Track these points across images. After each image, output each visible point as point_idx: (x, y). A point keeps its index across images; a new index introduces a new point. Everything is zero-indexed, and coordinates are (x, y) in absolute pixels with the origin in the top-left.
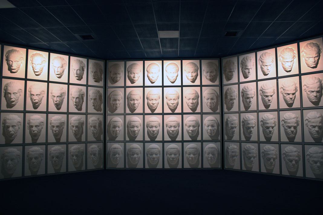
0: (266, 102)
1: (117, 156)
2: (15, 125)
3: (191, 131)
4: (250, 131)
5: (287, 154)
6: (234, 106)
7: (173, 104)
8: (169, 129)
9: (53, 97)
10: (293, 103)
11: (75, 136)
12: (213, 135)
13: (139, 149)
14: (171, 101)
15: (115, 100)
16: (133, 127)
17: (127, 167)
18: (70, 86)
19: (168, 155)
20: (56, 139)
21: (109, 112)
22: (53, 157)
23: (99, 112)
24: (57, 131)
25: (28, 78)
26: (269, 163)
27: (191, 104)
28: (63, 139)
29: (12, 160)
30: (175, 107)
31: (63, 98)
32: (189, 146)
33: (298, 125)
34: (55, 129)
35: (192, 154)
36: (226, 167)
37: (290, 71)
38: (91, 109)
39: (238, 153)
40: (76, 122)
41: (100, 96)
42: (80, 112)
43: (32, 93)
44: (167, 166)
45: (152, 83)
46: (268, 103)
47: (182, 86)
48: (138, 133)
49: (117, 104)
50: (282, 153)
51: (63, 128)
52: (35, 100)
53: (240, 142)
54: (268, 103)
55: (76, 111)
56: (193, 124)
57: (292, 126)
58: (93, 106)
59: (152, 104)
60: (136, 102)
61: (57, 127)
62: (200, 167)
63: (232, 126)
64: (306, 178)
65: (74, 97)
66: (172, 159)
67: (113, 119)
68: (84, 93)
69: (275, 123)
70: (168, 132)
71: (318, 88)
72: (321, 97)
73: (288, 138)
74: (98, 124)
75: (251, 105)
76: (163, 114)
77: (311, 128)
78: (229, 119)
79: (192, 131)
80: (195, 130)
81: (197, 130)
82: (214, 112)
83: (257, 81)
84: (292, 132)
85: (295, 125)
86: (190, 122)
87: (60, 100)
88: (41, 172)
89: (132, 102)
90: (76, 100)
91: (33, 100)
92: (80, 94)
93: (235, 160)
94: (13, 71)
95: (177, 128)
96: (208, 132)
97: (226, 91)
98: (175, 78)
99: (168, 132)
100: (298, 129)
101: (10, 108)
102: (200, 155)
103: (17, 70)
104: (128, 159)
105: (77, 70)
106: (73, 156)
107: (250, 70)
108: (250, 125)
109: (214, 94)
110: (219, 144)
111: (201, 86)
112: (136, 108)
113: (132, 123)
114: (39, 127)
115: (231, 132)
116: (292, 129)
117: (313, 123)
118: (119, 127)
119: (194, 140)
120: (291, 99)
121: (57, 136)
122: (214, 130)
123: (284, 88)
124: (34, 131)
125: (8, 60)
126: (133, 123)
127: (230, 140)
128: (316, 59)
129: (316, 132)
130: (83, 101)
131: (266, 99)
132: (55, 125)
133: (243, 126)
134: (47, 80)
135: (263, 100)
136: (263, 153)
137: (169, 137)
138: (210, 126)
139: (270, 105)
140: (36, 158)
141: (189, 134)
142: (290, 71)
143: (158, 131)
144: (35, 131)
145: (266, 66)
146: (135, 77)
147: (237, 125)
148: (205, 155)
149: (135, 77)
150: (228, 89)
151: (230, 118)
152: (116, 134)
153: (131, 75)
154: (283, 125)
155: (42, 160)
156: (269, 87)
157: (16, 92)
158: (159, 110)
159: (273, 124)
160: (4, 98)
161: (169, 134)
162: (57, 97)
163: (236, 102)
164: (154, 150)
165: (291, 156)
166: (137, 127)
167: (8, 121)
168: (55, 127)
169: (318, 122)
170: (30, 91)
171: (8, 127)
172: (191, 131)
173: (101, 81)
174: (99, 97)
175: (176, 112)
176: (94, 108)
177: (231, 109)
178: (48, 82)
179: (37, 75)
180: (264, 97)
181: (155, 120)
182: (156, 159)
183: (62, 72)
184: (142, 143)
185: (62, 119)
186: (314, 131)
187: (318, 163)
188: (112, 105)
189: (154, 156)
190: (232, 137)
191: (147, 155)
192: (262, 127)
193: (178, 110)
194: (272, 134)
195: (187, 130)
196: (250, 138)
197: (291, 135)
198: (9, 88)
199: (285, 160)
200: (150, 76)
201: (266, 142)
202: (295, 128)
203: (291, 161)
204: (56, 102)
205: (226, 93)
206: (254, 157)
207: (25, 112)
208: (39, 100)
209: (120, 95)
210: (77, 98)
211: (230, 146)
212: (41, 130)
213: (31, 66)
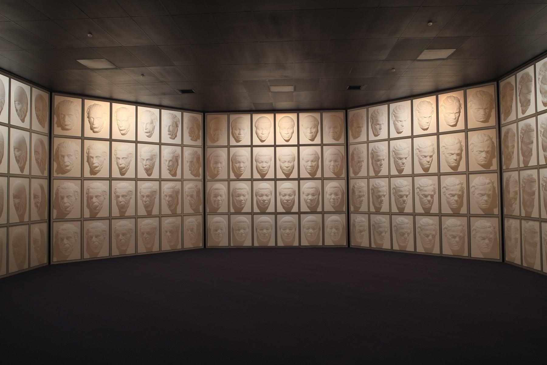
0: (399, 166)
1: (219, 231)
2: (100, 195)
3: (309, 201)
4: (380, 200)
5: (423, 227)
6: (362, 170)
7: (287, 167)
8: (283, 198)
10: (430, 167)
11: (169, 208)
12: (337, 205)
13: (246, 222)
14: (285, 163)
15: (216, 163)
16: (239, 195)
17: (232, 245)
19: (282, 230)
20: (147, 211)
21: (208, 178)
22: (143, 234)
23: (197, 178)
24: (148, 202)
26: (403, 238)
27: (311, 168)
28: (155, 212)
30: (290, 171)
31: (154, 162)
32: (307, 219)
33: (435, 193)
34: (144, 199)
35: (310, 229)
36: (352, 245)
37: (427, 129)
38: (188, 175)
39: (367, 228)
40: (170, 190)
41: (198, 159)
42: (174, 178)
43: (117, 156)
44: (280, 244)
45: (262, 141)
46: (402, 166)
47: (298, 145)
48: (245, 203)
49: (218, 168)
50: (417, 226)
51: (155, 198)
52: (120, 165)
53: (369, 213)
54: (402, 166)
55: (170, 177)
56: (312, 192)
57: (429, 195)
58: (190, 170)
59: (262, 167)
60: (242, 165)
61: (148, 196)
62: (320, 244)
63: (360, 194)
64: (443, 256)
66: (286, 235)
67: (213, 187)
68: (179, 154)
69: (409, 191)
70: (282, 202)
71: (458, 150)
72: (461, 161)
73: (424, 209)
74: (196, 193)
75: (382, 168)
76: (275, 180)
77: (449, 196)
78: (356, 186)
79: (311, 200)
80: (314, 199)
81: (316, 200)
82: (337, 178)
83: (389, 140)
84: (429, 201)
85: (433, 193)
86: (309, 189)
87: (150, 164)
88: (130, 251)
89: (237, 165)
90: (169, 163)
91: (118, 165)
93: (363, 236)
94: (95, 130)
95: (293, 197)
96: (330, 202)
97: (353, 151)
98: (290, 134)
99: (282, 202)
100: (434, 198)
101: (94, 175)
102: (320, 229)
106: (167, 232)
107: (382, 125)
108: (381, 194)
109: (338, 154)
110: (344, 216)
111: (322, 145)
112: (242, 173)
113: (237, 190)
114: (126, 197)
115: (358, 202)
116: (429, 198)
117: (452, 190)
118: (221, 196)
119: (313, 212)
120: (428, 162)
121: (149, 207)
122: (337, 200)
123: (421, 149)
124: (120, 202)
125: (89, 117)
126: (240, 191)
127: (357, 212)
128: (457, 115)
129: (455, 201)
130: (178, 165)
131: (400, 161)
133: (373, 194)
135: (395, 162)
136: (396, 226)
137: (283, 208)
138: (333, 195)
139: (404, 169)
140: (124, 235)
141: (308, 204)
142: (427, 129)
143: (269, 201)
144: (122, 202)
145: (401, 121)
146: (240, 134)
147: (366, 193)
148: (327, 230)
149: (240, 134)
150: (355, 149)
151: (357, 184)
152: (218, 205)
153: (236, 131)
154: (418, 193)
155: (131, 236)
156: (404, 146)
157: (100, 155)
158: (270, 175)
159: (408, 191)
160: (87, 163)
161: (283, 203)
162: (147, 160)
163: (364, 164)
164: (265, 223)
165: (427, 230)
166: (244, 196)
167: (91, 190)
168: (145, 197)
169: (458, 190)
170: (115, 154)
171: (92, 198)
172: (309, 201)
173: (199, 139)
174: (197, 159)
175: (291, 177)
176: (191, 173)
177: (358, 174)
178: (136, 142)
179: (123, 134)
180: (397, 160)
181: (266, 187)
182: (267, 235)
184: (227, 216)
185: (154, 187)
186: (453, 201)
187: (457, 237)
188: (213, 168)
189: (265, 231)
190: (360, 208)
191: (256, 229)
192: (394, 196)
193: (294, 175)
194: (406, 204)
195: (305, 199)
196: (380, 208)
197: (427, 205)
198: (91, 151)
199: (420, 235)
200: (260, 132)
201: (375, 213)
202: (432, 196)
203: (427, 236)
204: (145, 167)
205: (353, 153)
206: (386, 232)
207: (110, 179)
208: (126, 164)
209: (221, 156)
210: (170, 161)
211: (358, 219)
212: (130, 201)
213: (117, 123)
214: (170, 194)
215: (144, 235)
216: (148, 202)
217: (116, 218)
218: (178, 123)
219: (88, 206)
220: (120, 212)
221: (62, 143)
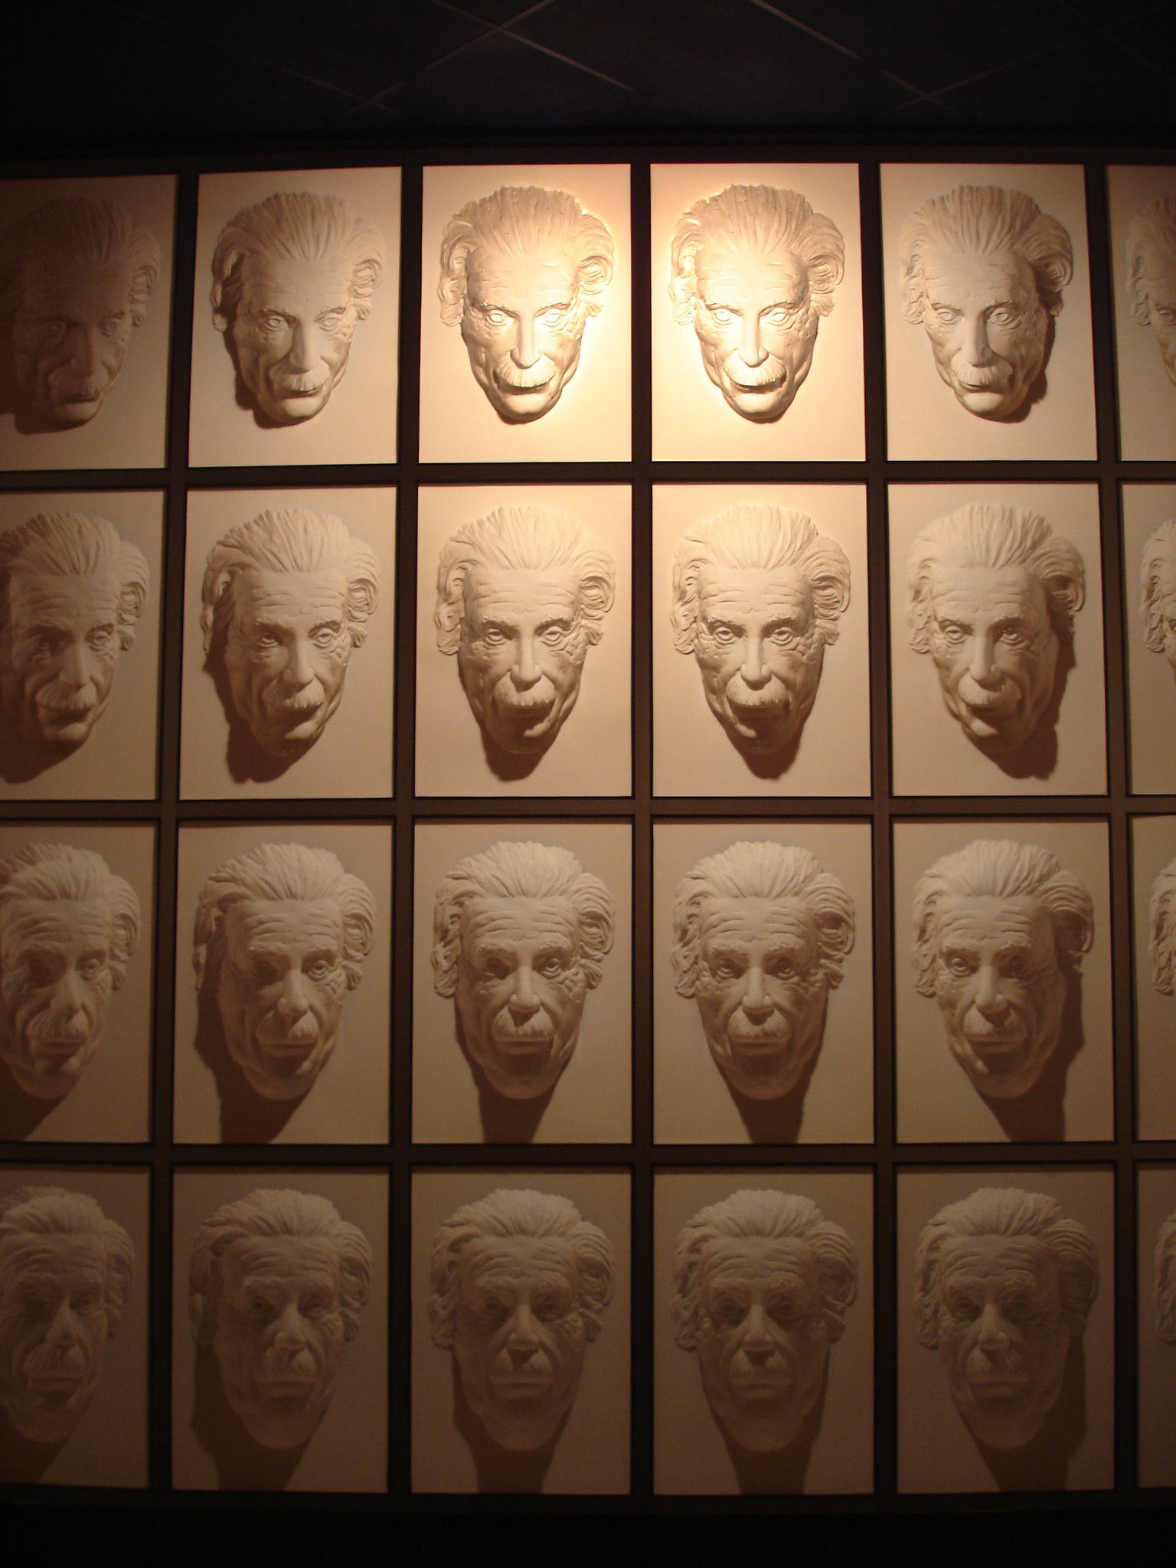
2: (332, 945)
9: (708, 641)
18: (898, 494)
25: (860, 456)
29: (312, 1303)
40: (1003, 905)
51: (833, 980)
61: (778, 964)
65: (960, 615)
87: (794, 666)
90: (990, 656)
92: (1033, 579)
94: (521, 403)
103: (553, 385)
104: (206, 1358)
105: (985, 315)
106: (968, 1307)
114: (565, 966)
124: (522, 1015)
130: (1066, 660)
132: (757, 949)
134: (626, 456)
140: (547, 1306)
155: (591, 1331)
162: (768, 630)
170: (456, 590)
171: (269, 970)
183: (796, 353)
208: (791, 675)
210: (997, 631)
213: (691, 328)
214: (1007, 940)
215: (736, 1323)
216: (775, 1021)
217: (202, 1158)
218: (1057, 268)
219: (211, 1044)
220: (491, 1102)
221: (480, 523)
